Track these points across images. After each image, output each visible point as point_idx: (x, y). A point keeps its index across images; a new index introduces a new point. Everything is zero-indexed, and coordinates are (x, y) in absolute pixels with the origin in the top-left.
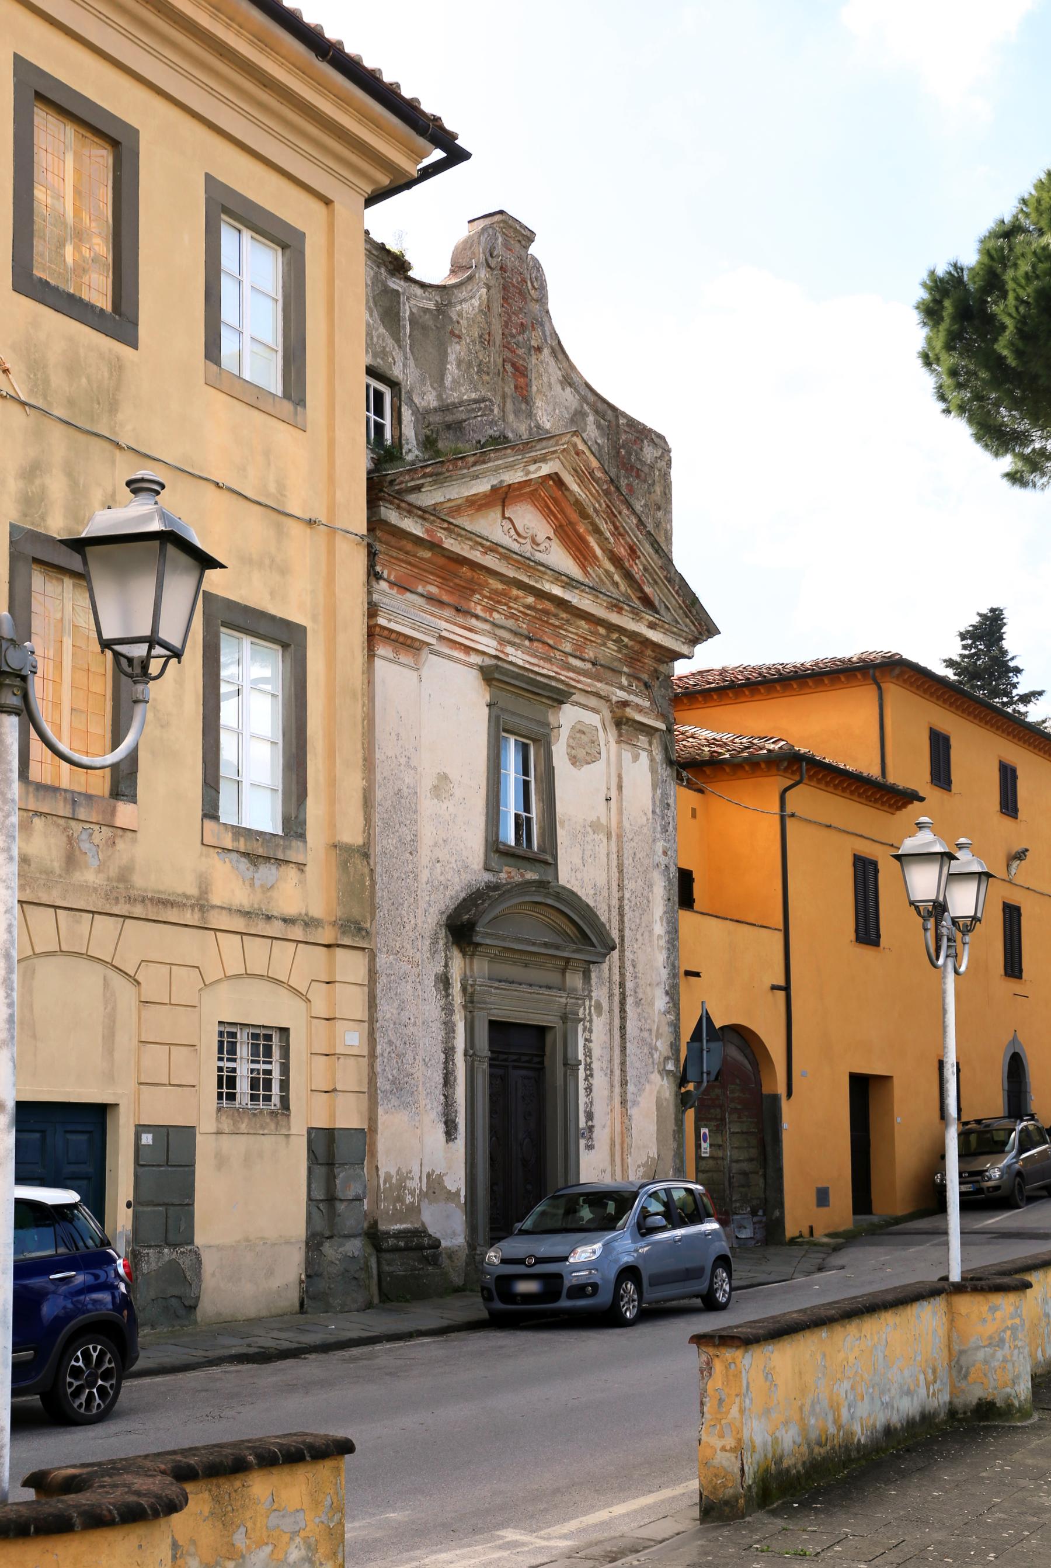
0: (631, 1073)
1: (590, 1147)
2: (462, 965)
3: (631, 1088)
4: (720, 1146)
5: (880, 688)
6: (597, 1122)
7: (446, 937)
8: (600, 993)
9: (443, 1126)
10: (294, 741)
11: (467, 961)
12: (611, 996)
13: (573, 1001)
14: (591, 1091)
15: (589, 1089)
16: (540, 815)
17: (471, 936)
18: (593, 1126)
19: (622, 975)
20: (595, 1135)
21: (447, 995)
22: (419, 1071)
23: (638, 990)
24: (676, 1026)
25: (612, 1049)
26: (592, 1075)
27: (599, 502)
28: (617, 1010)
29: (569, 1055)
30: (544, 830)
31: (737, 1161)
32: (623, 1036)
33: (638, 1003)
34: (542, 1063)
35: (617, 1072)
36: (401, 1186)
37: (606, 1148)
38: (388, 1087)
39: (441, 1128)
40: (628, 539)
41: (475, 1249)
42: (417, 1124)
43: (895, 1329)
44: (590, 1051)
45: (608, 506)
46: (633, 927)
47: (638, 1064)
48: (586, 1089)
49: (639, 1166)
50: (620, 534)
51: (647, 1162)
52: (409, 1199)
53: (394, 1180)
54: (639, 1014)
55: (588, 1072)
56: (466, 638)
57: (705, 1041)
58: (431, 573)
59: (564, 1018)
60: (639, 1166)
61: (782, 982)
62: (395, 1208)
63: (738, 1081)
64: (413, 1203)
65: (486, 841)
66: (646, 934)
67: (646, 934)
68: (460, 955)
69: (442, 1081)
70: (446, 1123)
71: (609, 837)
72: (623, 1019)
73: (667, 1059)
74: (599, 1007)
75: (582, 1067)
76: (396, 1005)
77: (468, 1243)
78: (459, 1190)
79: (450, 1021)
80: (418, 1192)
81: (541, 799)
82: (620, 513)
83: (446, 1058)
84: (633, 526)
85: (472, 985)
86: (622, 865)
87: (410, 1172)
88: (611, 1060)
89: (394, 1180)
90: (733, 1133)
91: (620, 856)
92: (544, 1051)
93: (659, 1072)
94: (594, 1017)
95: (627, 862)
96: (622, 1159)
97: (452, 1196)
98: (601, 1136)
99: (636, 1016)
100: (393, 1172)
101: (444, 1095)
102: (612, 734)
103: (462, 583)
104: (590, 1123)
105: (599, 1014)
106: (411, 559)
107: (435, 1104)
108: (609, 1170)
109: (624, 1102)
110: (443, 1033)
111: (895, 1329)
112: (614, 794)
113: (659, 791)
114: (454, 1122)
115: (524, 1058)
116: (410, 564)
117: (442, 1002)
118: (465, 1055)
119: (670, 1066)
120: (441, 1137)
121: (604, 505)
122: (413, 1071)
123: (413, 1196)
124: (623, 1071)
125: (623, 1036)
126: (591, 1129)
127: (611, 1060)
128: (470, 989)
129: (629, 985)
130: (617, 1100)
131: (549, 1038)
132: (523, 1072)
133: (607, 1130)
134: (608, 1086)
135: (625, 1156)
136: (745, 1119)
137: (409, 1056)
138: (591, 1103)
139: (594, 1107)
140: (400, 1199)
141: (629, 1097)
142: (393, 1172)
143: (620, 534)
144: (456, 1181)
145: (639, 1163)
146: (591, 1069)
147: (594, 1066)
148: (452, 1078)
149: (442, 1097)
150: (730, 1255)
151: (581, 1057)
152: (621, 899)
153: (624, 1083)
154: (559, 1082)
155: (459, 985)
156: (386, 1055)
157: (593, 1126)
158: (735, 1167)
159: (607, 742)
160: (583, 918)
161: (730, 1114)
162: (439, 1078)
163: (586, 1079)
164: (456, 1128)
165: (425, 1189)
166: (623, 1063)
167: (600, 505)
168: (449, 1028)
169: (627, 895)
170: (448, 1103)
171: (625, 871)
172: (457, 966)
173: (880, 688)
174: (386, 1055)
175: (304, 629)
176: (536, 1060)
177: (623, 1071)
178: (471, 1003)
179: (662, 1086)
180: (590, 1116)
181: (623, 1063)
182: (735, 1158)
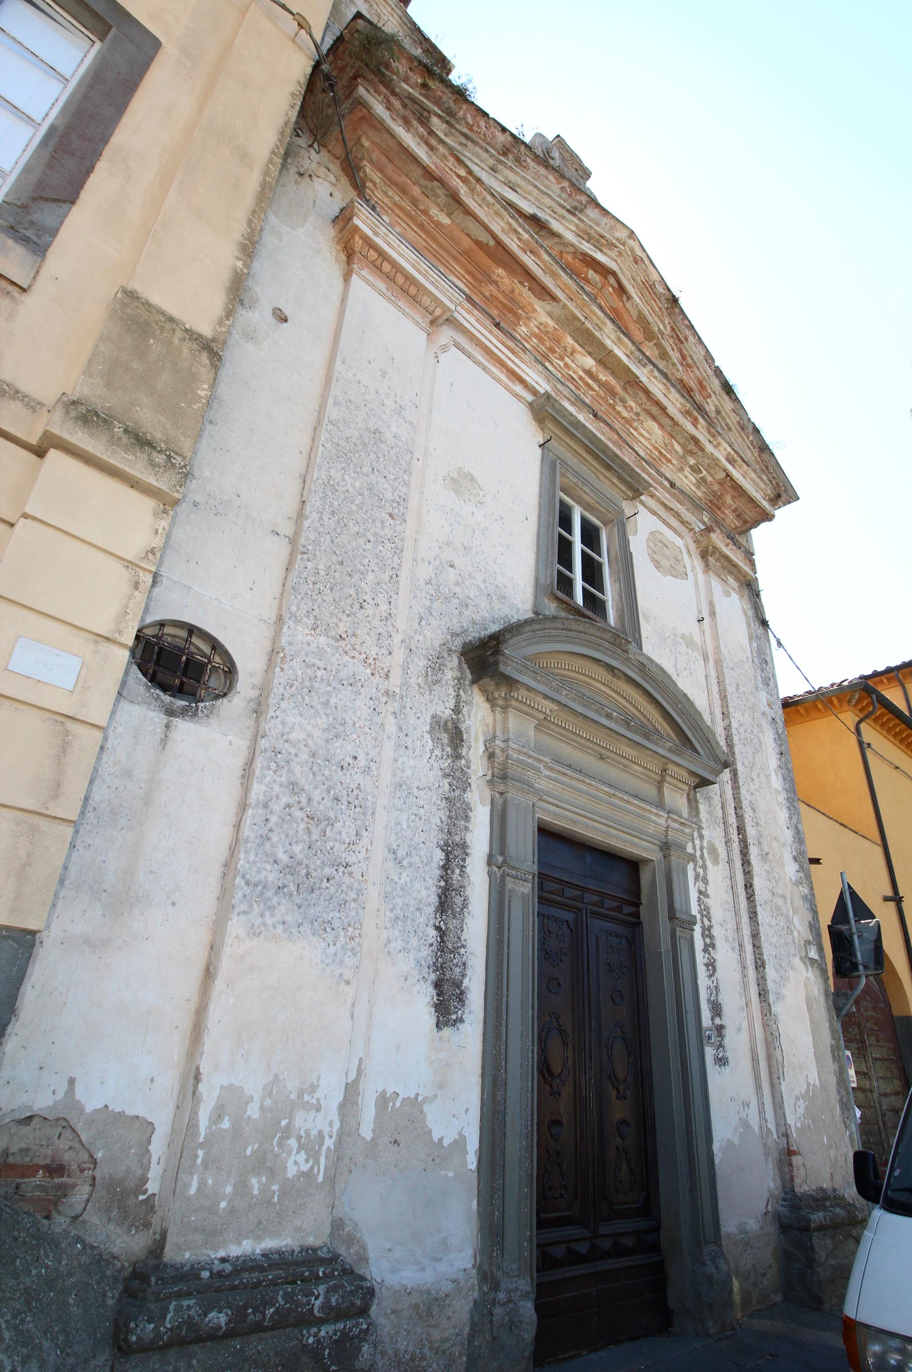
0: (768, 952)
1: (722, 1061)
2: (490, 720)
3: (770, 973)
4: (865, 1074)
5: (904, 688)
7: (460, 668)
8: (713, 834)
9: (431, 991)
11: (499, 716)
12: (728, 842)
13: (677, 826)
14: (715, 970)
15: (711, 966)
16: (617, 597)
17: (496, 663)
19: (740, 817)
20: (727, 1041)
21: (457, 757)
22: (373, 865)
23: (761, 840)
24: (811, 901)
25: (737, 913)
27: (663, 323)
28: (738, 862)
29: (677, 905)
30: (623, 612)
31: (885, 1095)
32: (751, 897)
33: (764, 856)
34: (637, 915)
35: (749, 948)
36: (276, 1127)
37: (746, 1065)
38: (271, 876)
39: (425, 995)
40: (697, 373)
41: (495, 1287)
42: (348, 974)
44: (707, 909)
45: (673, 329)
46: (746, 763)
47: (775, 940)
48: (707, 965)
50: (689, 366)
51: (808, 1091)
52: (296, 1163)
53: (253, 1111)
54: (768, 872)
55: (708, 940)
56: (509, 358)
57: (853, 922)
59: (666, 847)
60: (797, 1099)
61: (889, 893)
62: (242, 1186)
63: (868, 997)
64: (308, 1175)
65: (537, 580)
66: (762, 777)
67: (762, 777)
68: (487, 706)
69: (434, 900)
70: (438, 985)
71: (706, 658)
72: (748, 874)
73: (807, 942)
74: (713, 851)
75: (697, 929)
76: (322, 722)
77: (480, 1269)
78: (460, 1143)
79: (460, 798)
80: (329, 1143)
81: (616, 580)
82: (686, 339)
83: (448, 859)
84: (702, 358)
85: (503, 750)
86: (725, 690)
87: (313, 1088)
88: (738, 929)
89: (253, 1111)
90: (875, 1059)
91: (720, 682)
92: (640, 899)
93: (801, 958)
94: (709, 863)
95: (731, 690)
96: (772, 1085)
97: (440, 1155)
98: (738, 1042)
99: (764, 874)
100: (253, 1084)
101: (438, 928)
102: (698, 564)
105: (716, 861)
107: (414, 941)
108: (754, 1103)
109: (763, 994)
110: (443, 814)
112: (706, 615)
113: (755, 644)
114: (458, 984)
115: (609, 903)
117: (446, 763)
118: (490, 863)
119: (813, 954)
120: (426, 1016)
121: (669, 328)
122: (351, 859)
123: (313, 1155)
124: (757, 947)
125: (751, 897)
126: (720, 1029)
127: (738, 929)
128: (500, 757)
129: (751, 831)
130: (753, 990)
131: (645, 877)
132: (607, 925)
133: (744, 1036)
134: (738, 967)
135: (775, 1081)
136: (882, 1043)
137: (346, 828)
140: (265, 1164)
141: (770, 986)
142: (253, 1084)
143: (689, 366)
144: (457, 1117)
146: (711, 937)
147: (715, 932)
148: (458, 900)
149: (433, 933)
151: (694, 910)
152: (728, 728)
153: (760, 965)
154: (665, 945)
155: (482, 748)
156: (277, 807)
158: (885, 1102)
159: (693, 569)
160: (681, 712)
161: (868, 1036)
162: (429, 895)
163: (705, 950)
164: (461, 998)
165: (367, 1132)
166: (755, 935)
167: (665, 328)
168: (458, 813)
169: (734, 725)
170: (446, 946)
171: (729, 697)
172: (479, 717)
173: (904, 688)
174: (277, 807)
175: (156, 44)
176: (628, 909)
177: (757, 947)
178: (501, 776)
179: (808, 979)
180: (717, 1009)
181: (755, 935)
182: (883, 1091)
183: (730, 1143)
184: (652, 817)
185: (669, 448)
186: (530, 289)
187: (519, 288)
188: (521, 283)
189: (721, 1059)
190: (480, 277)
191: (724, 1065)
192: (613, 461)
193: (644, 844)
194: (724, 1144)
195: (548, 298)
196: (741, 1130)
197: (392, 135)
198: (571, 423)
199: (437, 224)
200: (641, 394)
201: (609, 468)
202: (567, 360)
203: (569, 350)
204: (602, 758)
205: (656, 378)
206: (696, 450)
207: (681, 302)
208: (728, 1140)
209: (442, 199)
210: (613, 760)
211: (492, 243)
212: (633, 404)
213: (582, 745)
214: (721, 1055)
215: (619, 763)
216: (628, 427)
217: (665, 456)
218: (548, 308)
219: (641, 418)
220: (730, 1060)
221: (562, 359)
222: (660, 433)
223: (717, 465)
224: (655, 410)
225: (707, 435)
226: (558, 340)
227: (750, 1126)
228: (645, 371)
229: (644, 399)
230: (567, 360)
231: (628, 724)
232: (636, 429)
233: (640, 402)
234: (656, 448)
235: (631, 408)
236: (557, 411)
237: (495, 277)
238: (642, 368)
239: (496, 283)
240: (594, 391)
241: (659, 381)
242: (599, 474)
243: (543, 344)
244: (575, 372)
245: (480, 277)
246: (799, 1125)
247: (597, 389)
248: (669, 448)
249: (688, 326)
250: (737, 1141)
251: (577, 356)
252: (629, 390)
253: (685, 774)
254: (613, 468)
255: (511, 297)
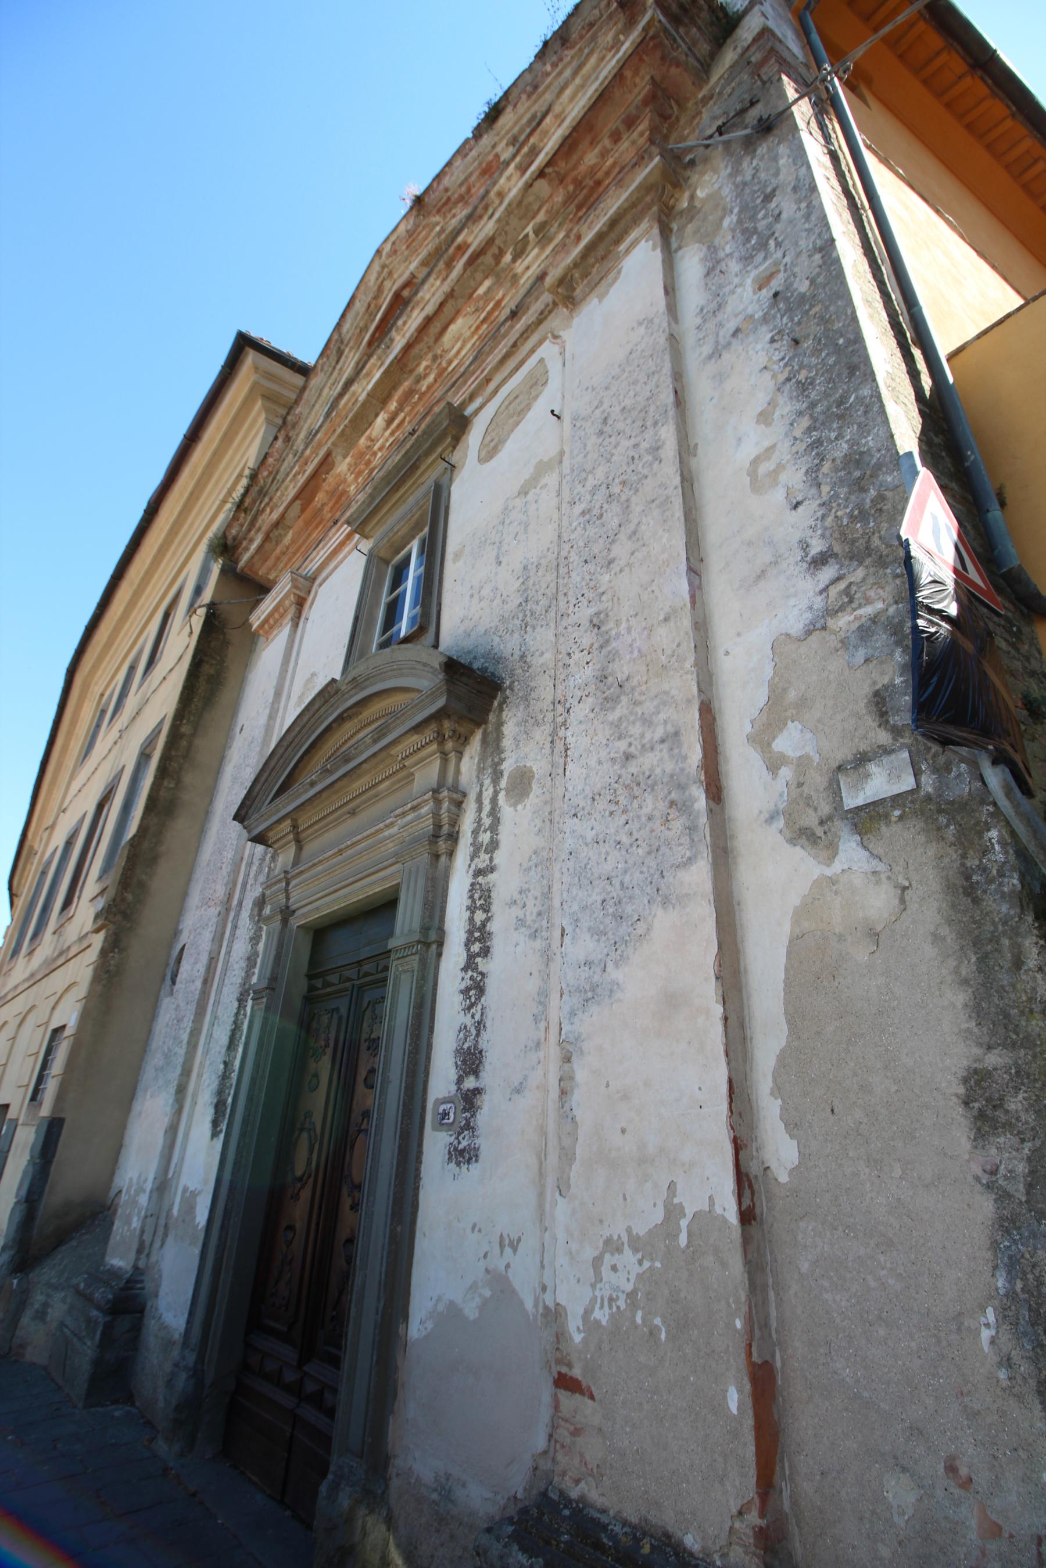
1: (463, 1155)
6: (492, 1077)
10: (745, 1001)
15: (475, 990)
18: (477, 1091)
20: (482, 1118)
26: (485, 952)
43: (537, 834)
49: (612, 1246)
58: (310, 535)
103: (331, 504)
104: (470, 1083)
106: (291, 550)
111: (537, 834)
116: (295, 553)
126: (470, 1100)
138: (480, 1026)
139: (485, 1036)
145: (617, 1229)
150: (626, 1246)
157: (477, 1091)
180: (471, 1061)
183: (453, 1311)
184: (386, 833)
185: (481, 303)
186: (327, 473)
187: (326, 486)
188: (324, 480)
189: (462, 1152)
190: (319, 519)
191: (469, 1161)
192: (410, 459)
193: (389, 871)
194: (440, 1308)
195: (330, 459)
196: (487, 1293)
197: (252, 557)
198: (369, 505)
199: (293, 541)
200: (415, 351)
201: (414, 467)
202: (376, 448)
203: (369, 443)
204: (353, 813)
205: (405, 323)
206: (494, 250)
207: (418, 189)
208: (452, 1304)
209: (280, 531)
210: (365, 802)
211: (298, 502)
212: (424, 364)
213: (336, 820)
214: (464, 1143)
215: (370, 799)
216: (446, 374)
217: (490, 314)
218: (339, 458)
219: (439, 352)
220: (483, 1154)
221: (375, 454)
222: (460, 322)
223: (520, 203)
224: (434, 329)
225: (482, 223)
226: (362, 455)
227: (514, 1292)
228: (398, 338)
229: (421, 345)
230: (376, 448)
231: (327, 771)
232: (450, 362)
233: (426, 350)
234: (478, 328)
235: (427, 367)
236: (358, 517)
237: (319, 505)
238: (395, 342)
239: (323, 505)
240: (405, 418)
241: (409, 317)
242: (419, 481)
243: (363, 472)
244: (387, 440)
245: (319, 519)
246: (602, 1315)
247: (402, 415)
248: (481, 303)
249: (439, 183)
250: (471, 1311)
251: (374, 435)
252: (411, 366)
253: (415, 738)
254: (415, 463)
255: (331, 494)
